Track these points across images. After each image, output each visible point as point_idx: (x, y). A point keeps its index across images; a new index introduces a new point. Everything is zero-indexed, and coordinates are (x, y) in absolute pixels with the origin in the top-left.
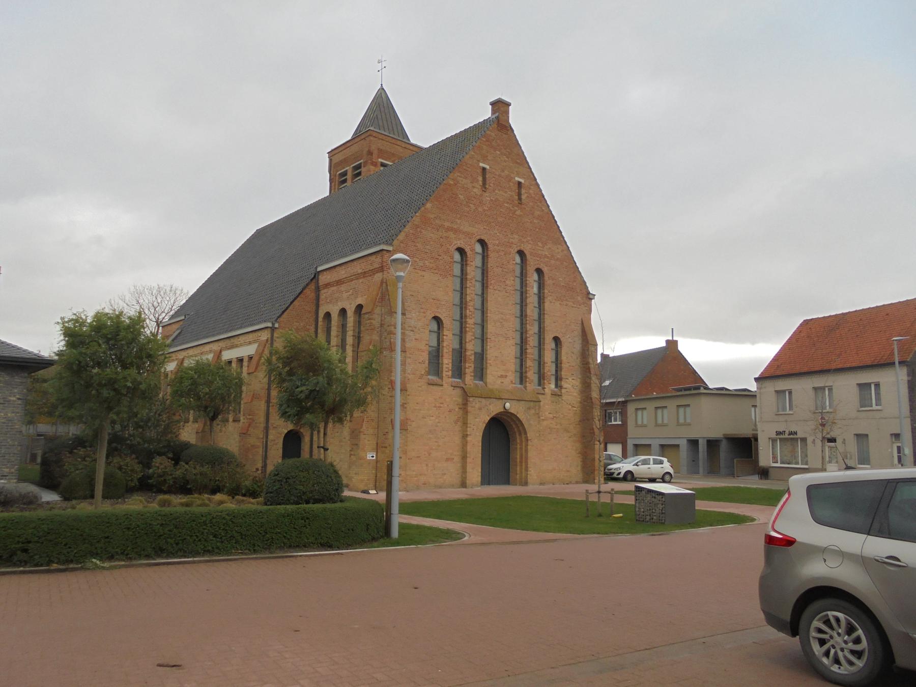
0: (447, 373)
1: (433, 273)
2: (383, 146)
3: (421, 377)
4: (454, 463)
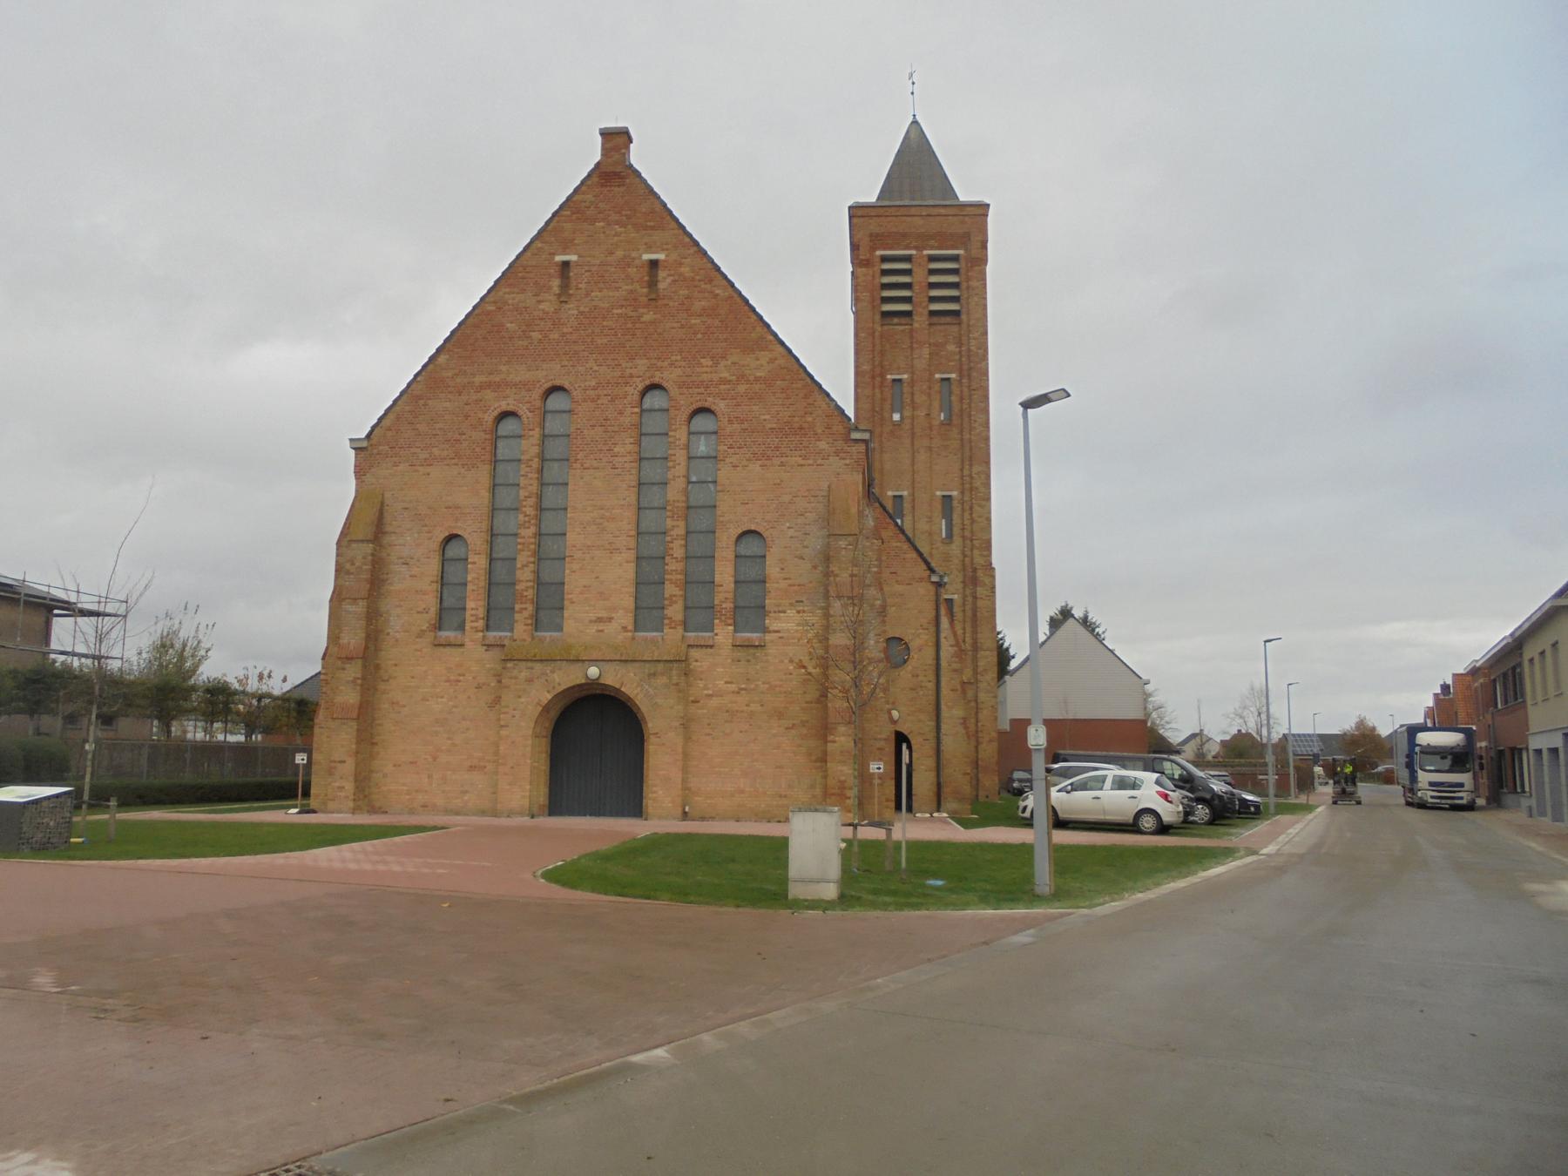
0: (475, 624)
1: (448, 465)
2: (881, 226)
3: (421, 634)
4: (485, 773)
